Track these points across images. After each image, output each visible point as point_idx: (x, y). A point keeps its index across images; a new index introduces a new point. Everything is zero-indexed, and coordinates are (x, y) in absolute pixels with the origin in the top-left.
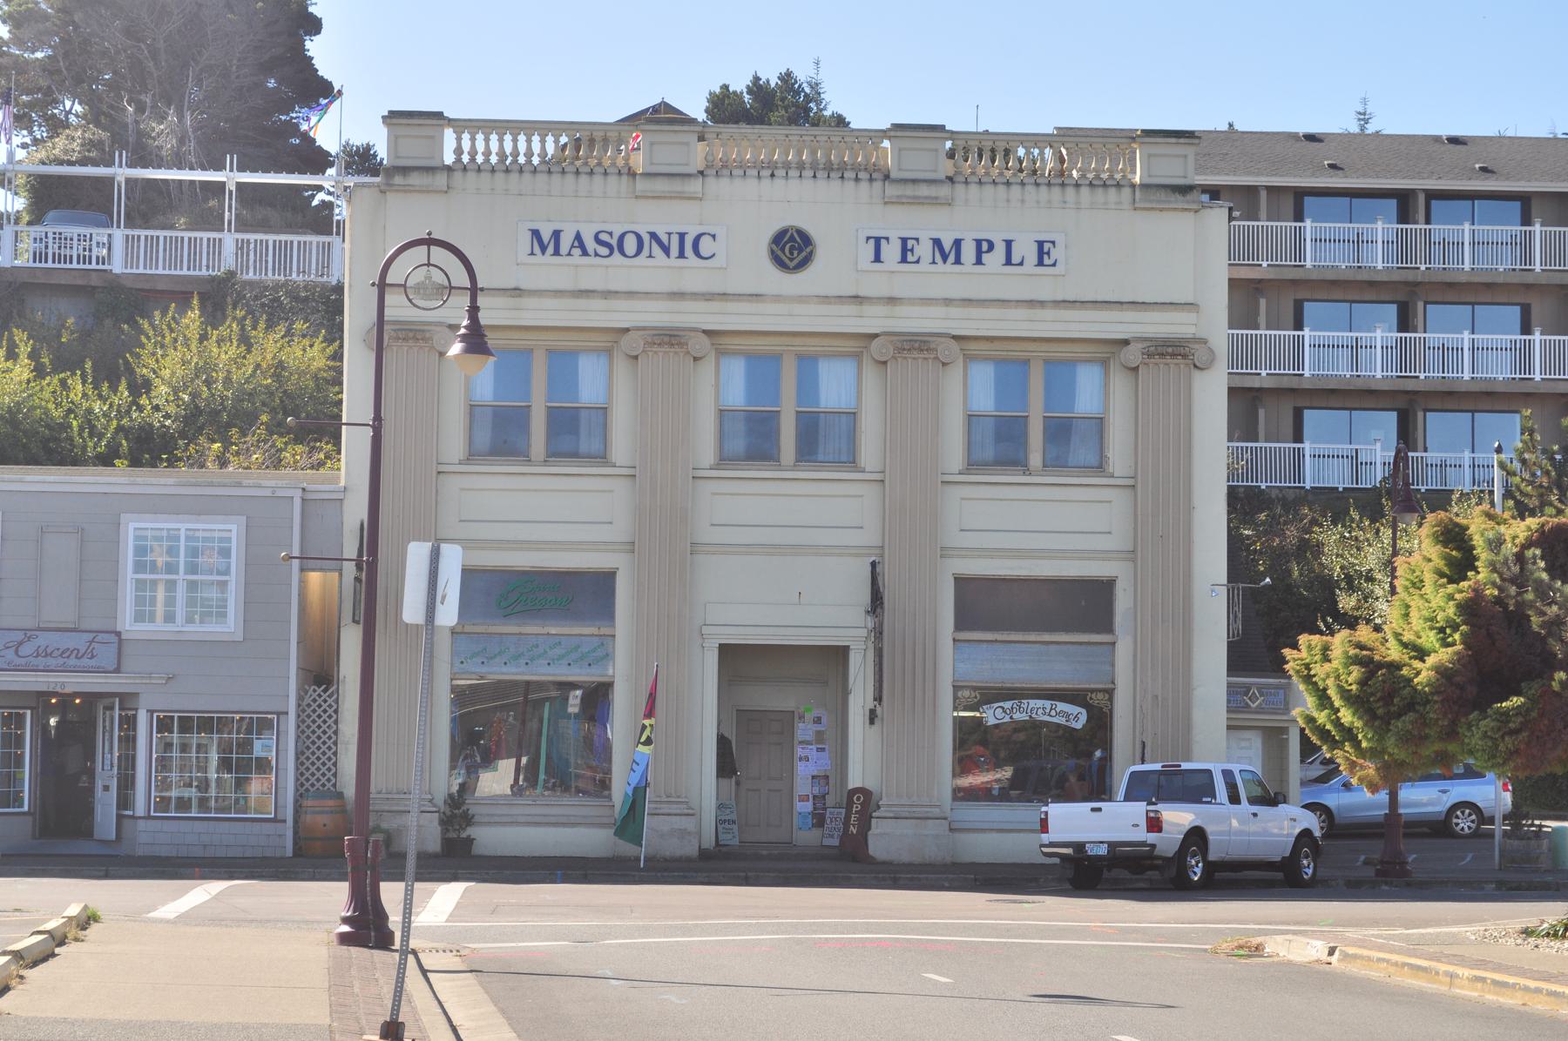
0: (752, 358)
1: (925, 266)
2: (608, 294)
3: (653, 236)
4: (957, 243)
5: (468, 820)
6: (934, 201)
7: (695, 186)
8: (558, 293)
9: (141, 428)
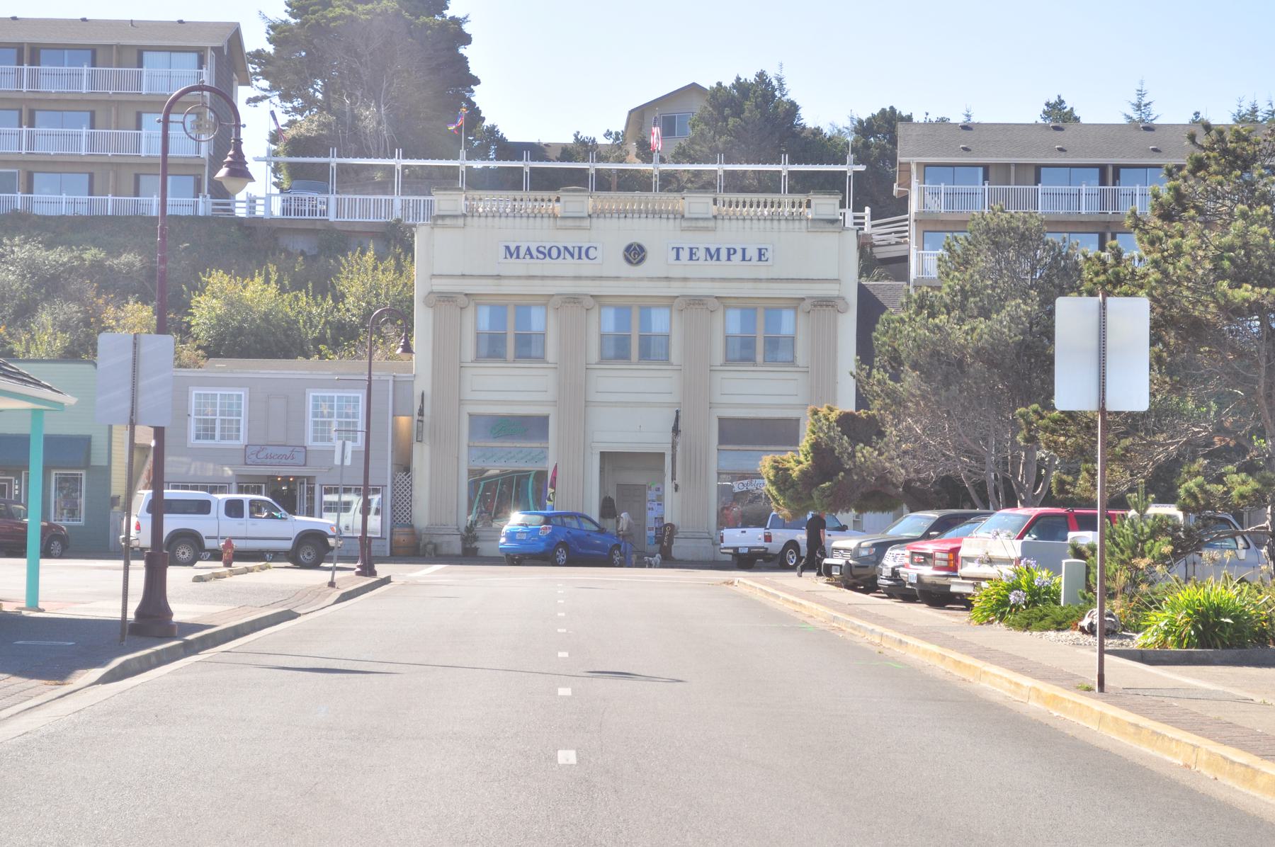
0: (618, 308)
1: (701, 261)
2: (543, 278)
3: (566, 248)
4: (718, 250)
5: (476, 539)
6: (706, 229)
7: (586, 223)
8: (519, 277)
9: (339, 321)
